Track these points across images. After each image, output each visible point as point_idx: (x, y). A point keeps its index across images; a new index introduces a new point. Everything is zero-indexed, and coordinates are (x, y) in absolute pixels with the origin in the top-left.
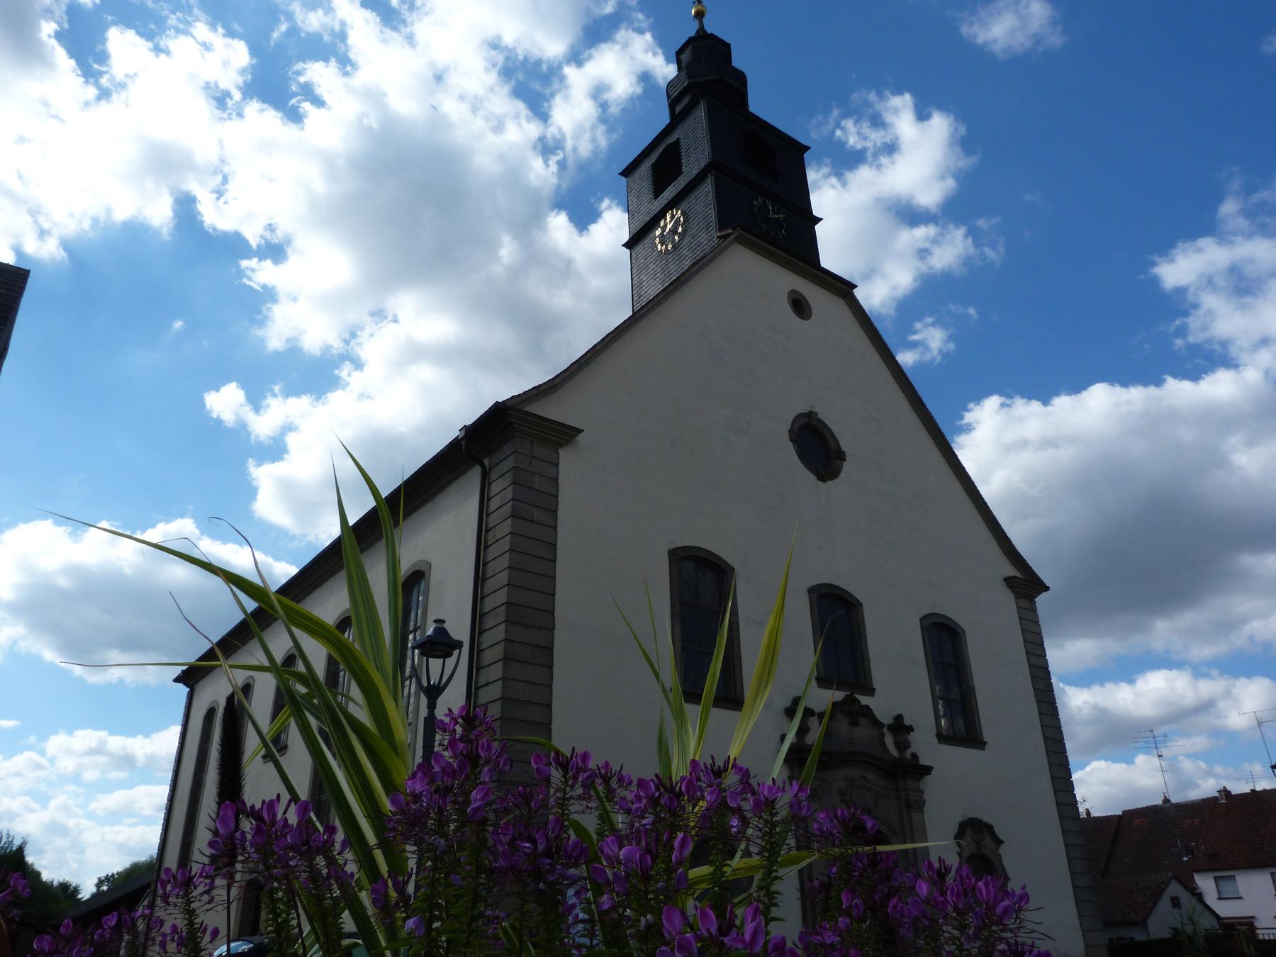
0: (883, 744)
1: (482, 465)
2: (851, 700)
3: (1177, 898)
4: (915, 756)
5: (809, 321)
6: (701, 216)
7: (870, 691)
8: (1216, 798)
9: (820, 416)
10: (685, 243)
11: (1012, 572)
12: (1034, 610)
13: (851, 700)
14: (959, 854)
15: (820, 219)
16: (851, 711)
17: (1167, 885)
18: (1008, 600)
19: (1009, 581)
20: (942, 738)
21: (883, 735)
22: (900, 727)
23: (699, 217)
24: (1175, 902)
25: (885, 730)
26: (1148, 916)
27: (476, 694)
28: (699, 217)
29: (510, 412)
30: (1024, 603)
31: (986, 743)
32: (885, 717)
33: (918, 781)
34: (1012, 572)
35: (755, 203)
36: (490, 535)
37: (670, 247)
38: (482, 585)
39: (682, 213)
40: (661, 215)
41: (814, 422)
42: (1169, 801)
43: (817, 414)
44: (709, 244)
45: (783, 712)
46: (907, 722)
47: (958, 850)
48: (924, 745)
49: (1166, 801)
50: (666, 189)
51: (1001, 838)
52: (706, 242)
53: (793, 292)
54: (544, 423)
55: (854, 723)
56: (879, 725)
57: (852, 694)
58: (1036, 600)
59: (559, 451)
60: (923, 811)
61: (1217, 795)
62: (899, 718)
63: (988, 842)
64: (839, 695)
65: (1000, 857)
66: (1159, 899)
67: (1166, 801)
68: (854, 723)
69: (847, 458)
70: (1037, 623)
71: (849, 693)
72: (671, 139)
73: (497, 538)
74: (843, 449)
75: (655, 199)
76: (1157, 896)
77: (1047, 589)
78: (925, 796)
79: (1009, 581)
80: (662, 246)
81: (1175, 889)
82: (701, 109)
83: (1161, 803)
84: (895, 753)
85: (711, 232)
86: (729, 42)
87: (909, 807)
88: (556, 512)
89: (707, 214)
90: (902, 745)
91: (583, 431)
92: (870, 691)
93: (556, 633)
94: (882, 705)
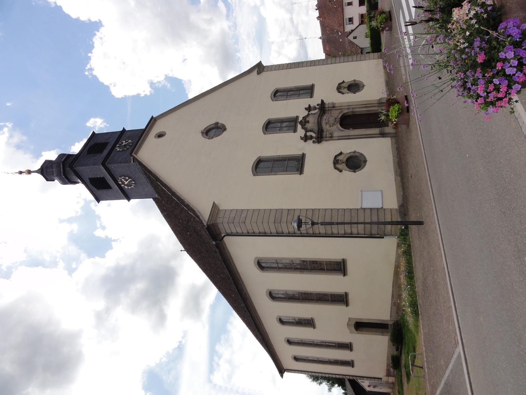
0: (314, 114)
1: (225, 236)
2: (301, 123)
3: (354, 37)
4: (318, 105)
5: (166, 132)
6: (123, 169)
7: (297, 117)
8: (320, 21)
9: (203, 129)
10: (133, 176)
11: (255, 72)
12: (268, 66)
13: (301, 123)
14: (348, 93)
15: (124, 128)
16: (304, 122)
17: (349, 40)
18: (264, 74)
19: (259, 73)
20: (311, 97)
21: (312, 114)
22: (309, 109)
23: (123, 170)
24: (355, 38)
25: (310, 113)
26: (359, 47)
27: (304, 234)
28: (123, 170)
29: (209, 224)
30: (265, 69)
31: (313, 84)
32: (306, 113)
33: (326, 104)
34: (255, 72)
35: (118, 150)
36: (250, 231)
37: (133, 182)
38: (267, 234)
39: (120, 177)
40: (119, 186)
41: (205, 132)
42: (321, 37)
43: (202, 131)
44: (135, 166)
45: (305, 143)
46: (307, 106)
47: (347, 94)
48: (315, 101)
49: (320, 38)
50: (109, 184)
51: (342, 81)
52: (134, 168)
53: (155, 137)
54: (212, 212)
55: (308, 122)
56: (308, 115)
57: (299, 122)
58: (264, 66)
59: (221, 209)
60: (335, 103)
61: (319, 21)
62: (306, 109)
63: (344, 85)
64: (299, 127)
65: (349, 82)
66: (354, 43)
67: (320, 38)
68: (308, 122)
69: (218, 121)
70: (272, 66)
71: (298, 123)
72: (88, 181)
73: (251, 228)
74: (214, 123)
75: (112, 188)
76: (353, 43)
77: (261, 61)
78: (330, 102)
79: (259, 73)
80: (132, 186)
81: (351, 37)
82: (78, 168)
83: (321, 40)
84: (317, 110)
85: (131, 165)
86: (45, 161)
87: (334, 107)
88: (242, 210)
89: (123, 167)
90: (315, 108)
91: (214, 202)
92: (297, 117)
93: (283, 208)
94: (302, 114)
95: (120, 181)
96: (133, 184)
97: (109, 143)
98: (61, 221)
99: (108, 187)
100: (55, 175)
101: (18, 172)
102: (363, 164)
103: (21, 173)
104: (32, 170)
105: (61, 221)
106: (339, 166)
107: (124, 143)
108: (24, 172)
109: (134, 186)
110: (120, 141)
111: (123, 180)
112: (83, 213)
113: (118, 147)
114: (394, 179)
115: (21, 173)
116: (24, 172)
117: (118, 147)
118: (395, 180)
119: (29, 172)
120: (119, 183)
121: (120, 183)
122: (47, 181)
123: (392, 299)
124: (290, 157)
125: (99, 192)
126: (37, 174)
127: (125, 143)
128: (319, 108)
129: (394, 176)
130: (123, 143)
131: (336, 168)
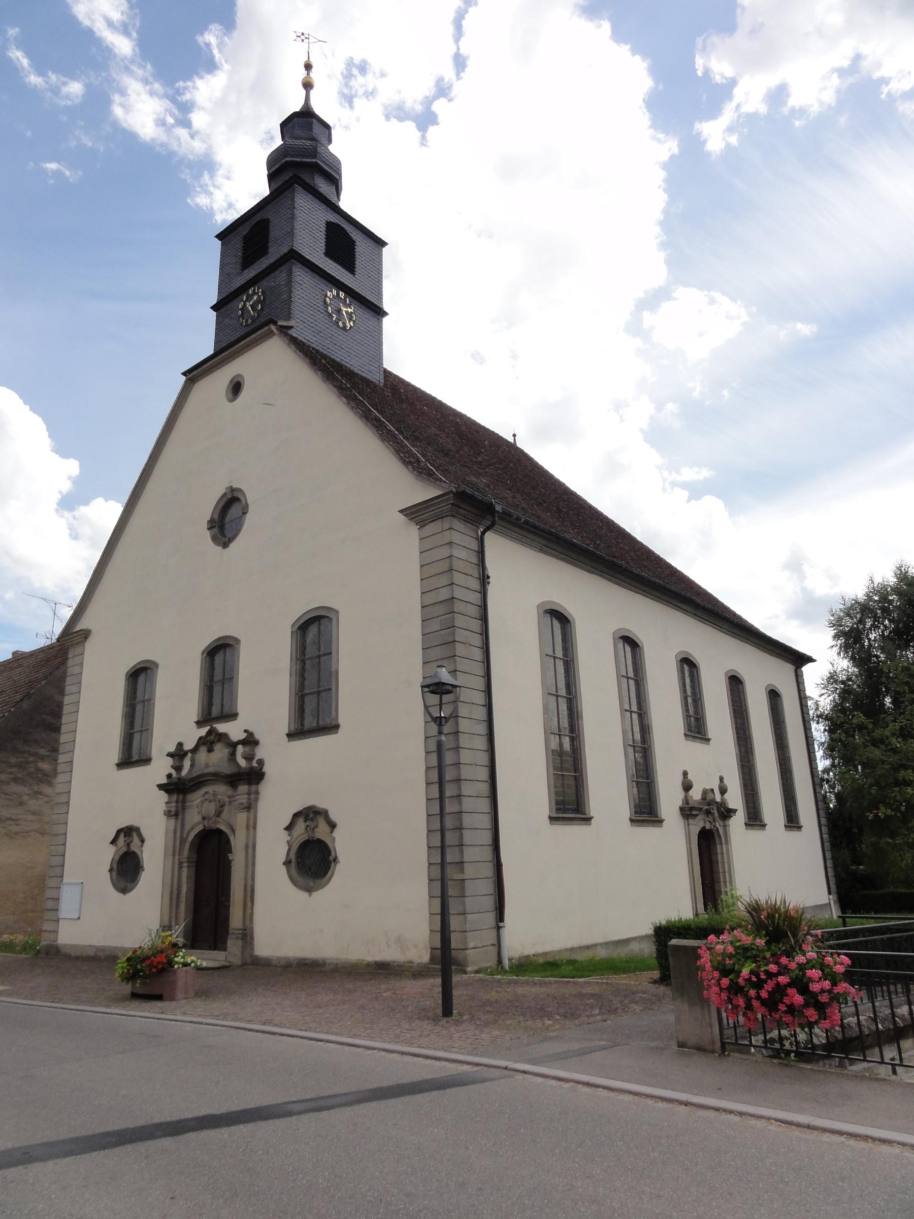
90: (249, 758)
95: (254, 290)
96: (247, 321)
97: (352, 276)
98: (721, 779)
99: (246, 263)
100: (290, 141)
101: (310, 59)
102: (115, 866)
103: (308, 67)
104: (312, 93)
105: (721, 779)
106: (301, 825)
107: (345, 309)
108: (308, 74)
109: (242, 324)
110: (352, 300)
111: (255, 298)
112: (214, 222)
113: (338, 294)
114: (93, 943)
115: (308, 67)
116: (308, 74)
117: (338, 294)
118: (91, 946)
119: (308, 85)
120: (250, 288)
121: (250, 292)
122: (281, 125)
123: (818, 906)
124: (295, 714)
125: (237, 242)
126: (303, 103)
127: (347, 312)
128: (252, 768)
129: (98, 945)
130: (346, 306)
131: (296, 816)
